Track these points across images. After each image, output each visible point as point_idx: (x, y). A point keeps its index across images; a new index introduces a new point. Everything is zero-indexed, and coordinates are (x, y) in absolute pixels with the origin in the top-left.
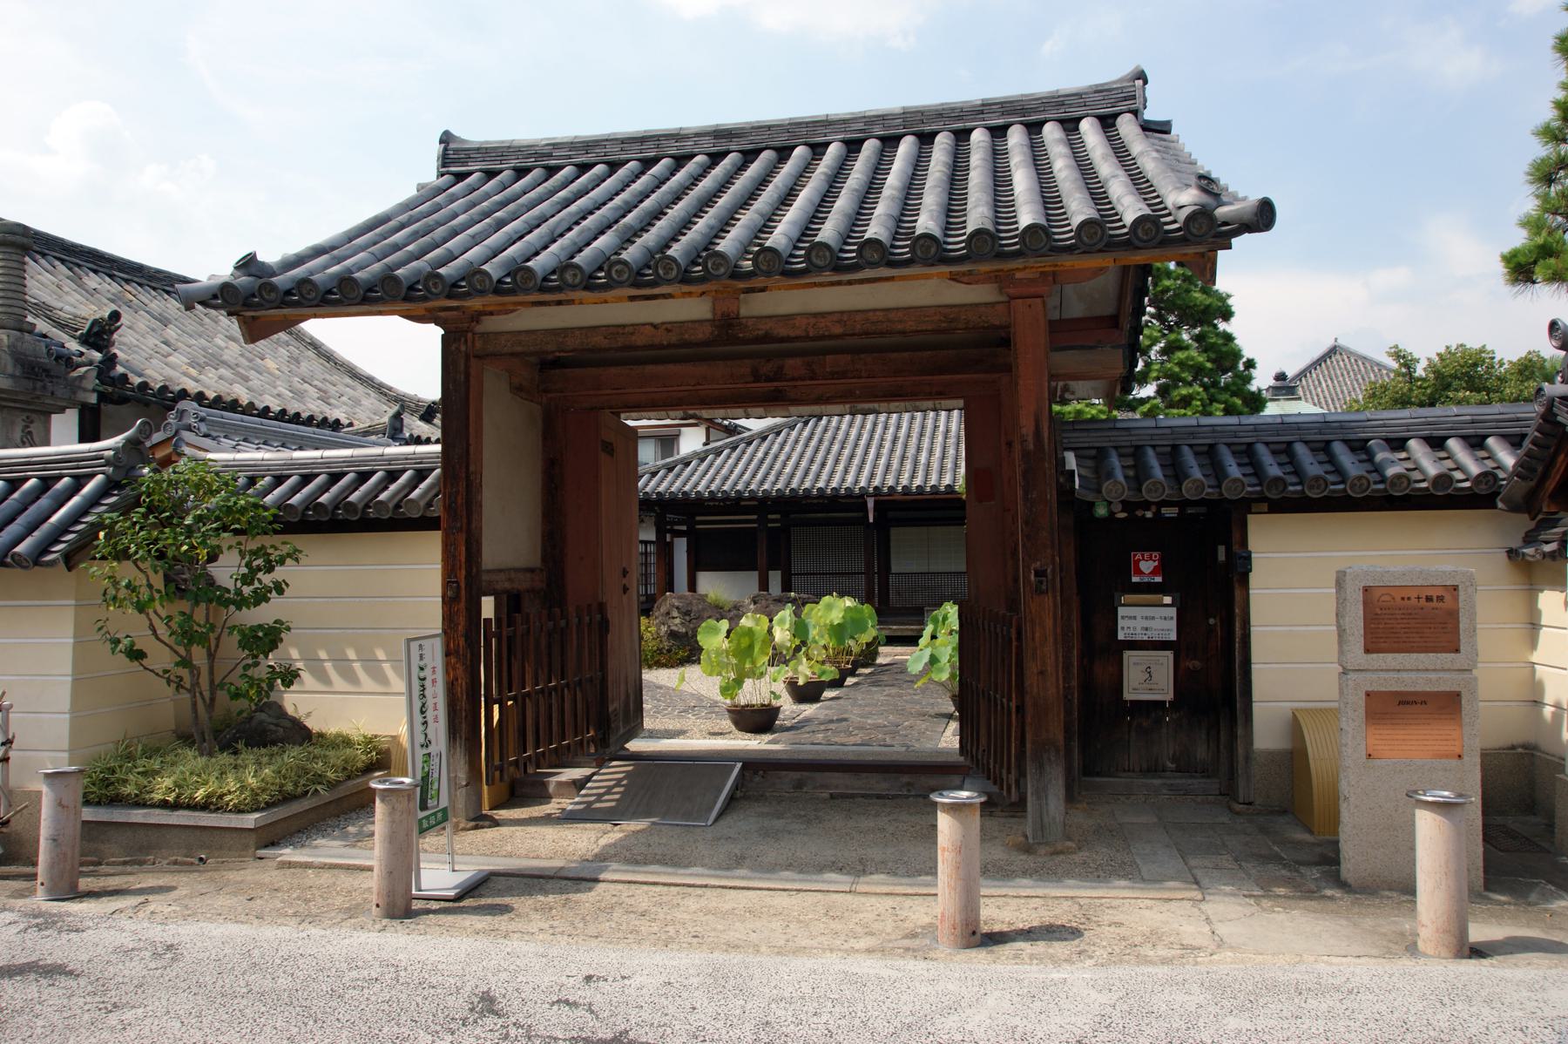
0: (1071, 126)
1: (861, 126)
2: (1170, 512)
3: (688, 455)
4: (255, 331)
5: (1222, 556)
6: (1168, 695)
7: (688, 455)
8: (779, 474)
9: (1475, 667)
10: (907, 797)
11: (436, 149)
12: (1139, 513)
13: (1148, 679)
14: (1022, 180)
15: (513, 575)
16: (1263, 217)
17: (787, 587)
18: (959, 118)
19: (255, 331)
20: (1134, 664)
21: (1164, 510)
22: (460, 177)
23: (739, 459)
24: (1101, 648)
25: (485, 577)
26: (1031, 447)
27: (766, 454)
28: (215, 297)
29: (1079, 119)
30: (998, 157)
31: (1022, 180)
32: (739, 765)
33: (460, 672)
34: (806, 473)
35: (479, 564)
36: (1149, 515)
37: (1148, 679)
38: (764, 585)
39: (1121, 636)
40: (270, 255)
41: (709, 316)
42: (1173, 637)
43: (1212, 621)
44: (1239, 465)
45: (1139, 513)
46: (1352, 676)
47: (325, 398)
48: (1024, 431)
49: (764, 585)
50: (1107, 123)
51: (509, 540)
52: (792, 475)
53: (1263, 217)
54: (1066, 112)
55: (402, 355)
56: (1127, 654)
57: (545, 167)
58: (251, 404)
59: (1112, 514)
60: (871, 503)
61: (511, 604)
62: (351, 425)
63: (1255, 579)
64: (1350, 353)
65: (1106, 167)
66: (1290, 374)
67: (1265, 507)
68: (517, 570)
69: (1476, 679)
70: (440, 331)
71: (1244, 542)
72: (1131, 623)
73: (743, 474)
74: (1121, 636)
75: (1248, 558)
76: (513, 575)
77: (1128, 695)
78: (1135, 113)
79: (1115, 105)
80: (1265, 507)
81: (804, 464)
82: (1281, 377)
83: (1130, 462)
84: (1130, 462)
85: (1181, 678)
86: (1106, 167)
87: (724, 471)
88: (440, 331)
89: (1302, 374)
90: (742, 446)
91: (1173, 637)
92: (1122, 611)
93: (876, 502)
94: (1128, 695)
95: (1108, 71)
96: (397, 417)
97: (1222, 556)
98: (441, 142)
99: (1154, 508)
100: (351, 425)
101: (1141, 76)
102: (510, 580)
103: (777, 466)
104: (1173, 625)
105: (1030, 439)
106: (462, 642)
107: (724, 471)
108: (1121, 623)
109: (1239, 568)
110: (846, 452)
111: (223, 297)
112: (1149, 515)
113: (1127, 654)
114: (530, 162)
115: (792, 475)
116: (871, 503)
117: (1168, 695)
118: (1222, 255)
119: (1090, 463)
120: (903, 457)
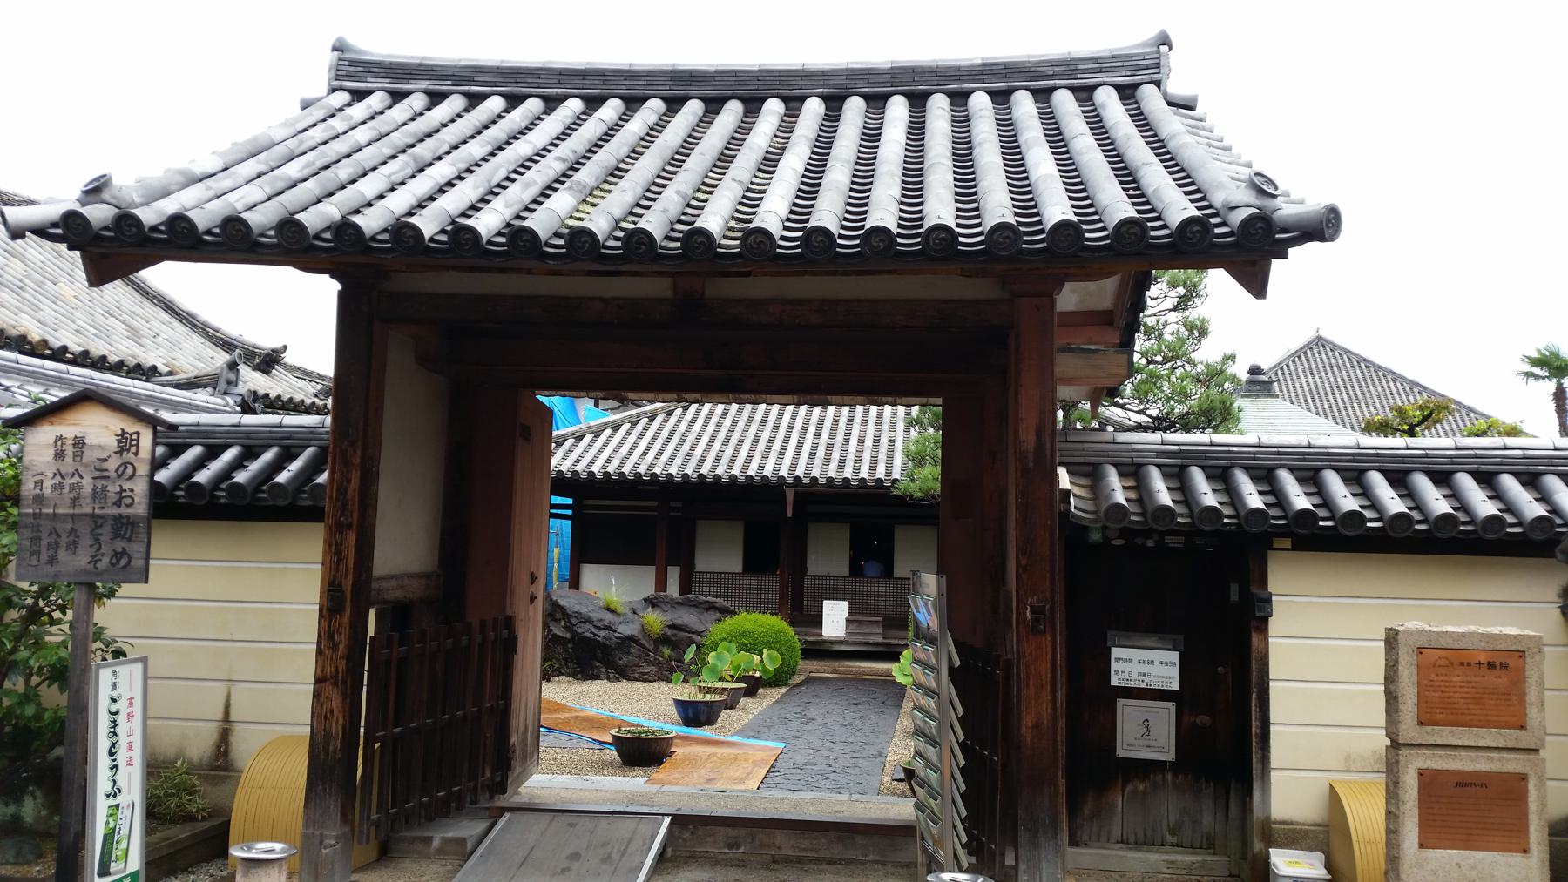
0: (1084, 95)
1: (842, 80)
2: (1174, 542)
3: (595, 438)
4: (99, 274)
5: (1234, 596)
6: (1167, 754)
7: (595, 438)
8: (689, 455)
9: (1543, 746)
10: (863, 863)
11: (329, 58)
12: (1139, 541)
13: (1147, 734)
14: (1042, 164)
15: (406, 582)
16: (1323, 227)
17: (685, 588)
18: (959, 80)
19: (99, 274)
20: (1129, 715)
21: (1167, 539)
22: (359, 95)
23: (641, 436)
24: (1095, 698)
25: (374, 585)
26: (1031, 465)
27: (672, 432)
28: (54, 225)
29: (1094, 88)
30: (1007, 129)
31: (1042, 164)
32: (668, 819)
33: (336, 704)
34: (718, 458)
35: (370, 569)
36: (1150, 543)
37: (1147, 734)
38: (661, 584)
39: (1114, 682)
40: (127, 181)
41: (669, 294)
42: (1176, 686)
43: (1220, 669)
44: (1260, 493)
45: (1139, 541)
46: (1403, 751)
47: (134, 334)
48: (1024, 446)
49: (661, 584)
50: (1127, 93)
51: (402, 546)
52: (703, 458)
53: (1323, 227)
54: (1080, 77)
55: (296, 318)
56: (1121, 702)
57: (467, 95)
58: (45, 342)
59: (1107, 540)
60: (790, 495)
61: (398, 615)
62: (171, 373)
63: (1274, 626)
64: (1334, 347)
65: (1138, 151)
66: (1265, 367)
67: (1288, 543)
68: (411, 576)
69: (1543, 760)
70: (336, 286)
71: (1264, 582)
72: (1126, 667)
73: (645, 453)
74: (1114, 682)
75: (1269, 601)
76: (406, 582)
77: (1121, 752)
78: (1158, 84)
79: (1135, 75)
80: (1288, 543)
81: (717, 446)
82: (1255, 370)
83: (1131, 483)
84: (1131, 483)
85: (1185, 736)
86: (1138, 151)
87: (624, 451)
88: (336, 286)
89: (1279, 368)
90: (644, 421)
91: (1176, 686)
92: (1116, 652)
93: (796, 494)
94: (1121, 752)
95: (1116, 34)
96: (233, 366)
97: (1234, 596)
98: (334, 49)
99: (1156, 537)
100: (171, 373)
101: (1164, 40)
102: (402, 587)
103: (686, 447)
104: (1175, 672)
105: (1031, 456)
106: (342, 664)
107: (624, 451)
108: (1114, 666)
109: (1253, 615)
110: (766, 435)
111: (69, 230)
112: (1150, 543)
113: (1121, 702)
114: (444, 86)
115: (703, 458)
116: (790, 495)
117: (1167, 754)
118: (1276, 264)
119: (1083, 481)
120: (830, 446)
